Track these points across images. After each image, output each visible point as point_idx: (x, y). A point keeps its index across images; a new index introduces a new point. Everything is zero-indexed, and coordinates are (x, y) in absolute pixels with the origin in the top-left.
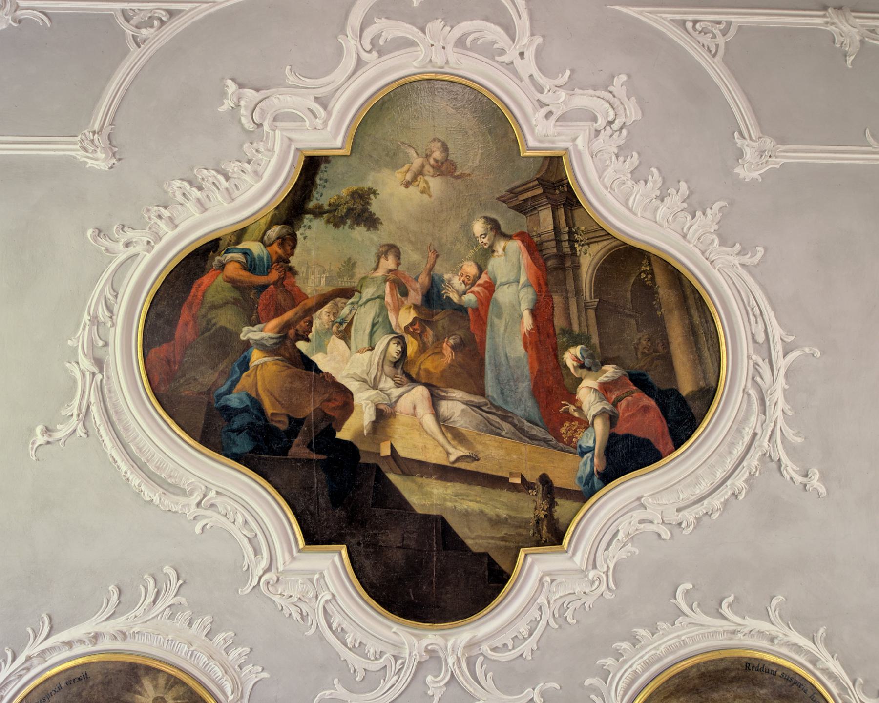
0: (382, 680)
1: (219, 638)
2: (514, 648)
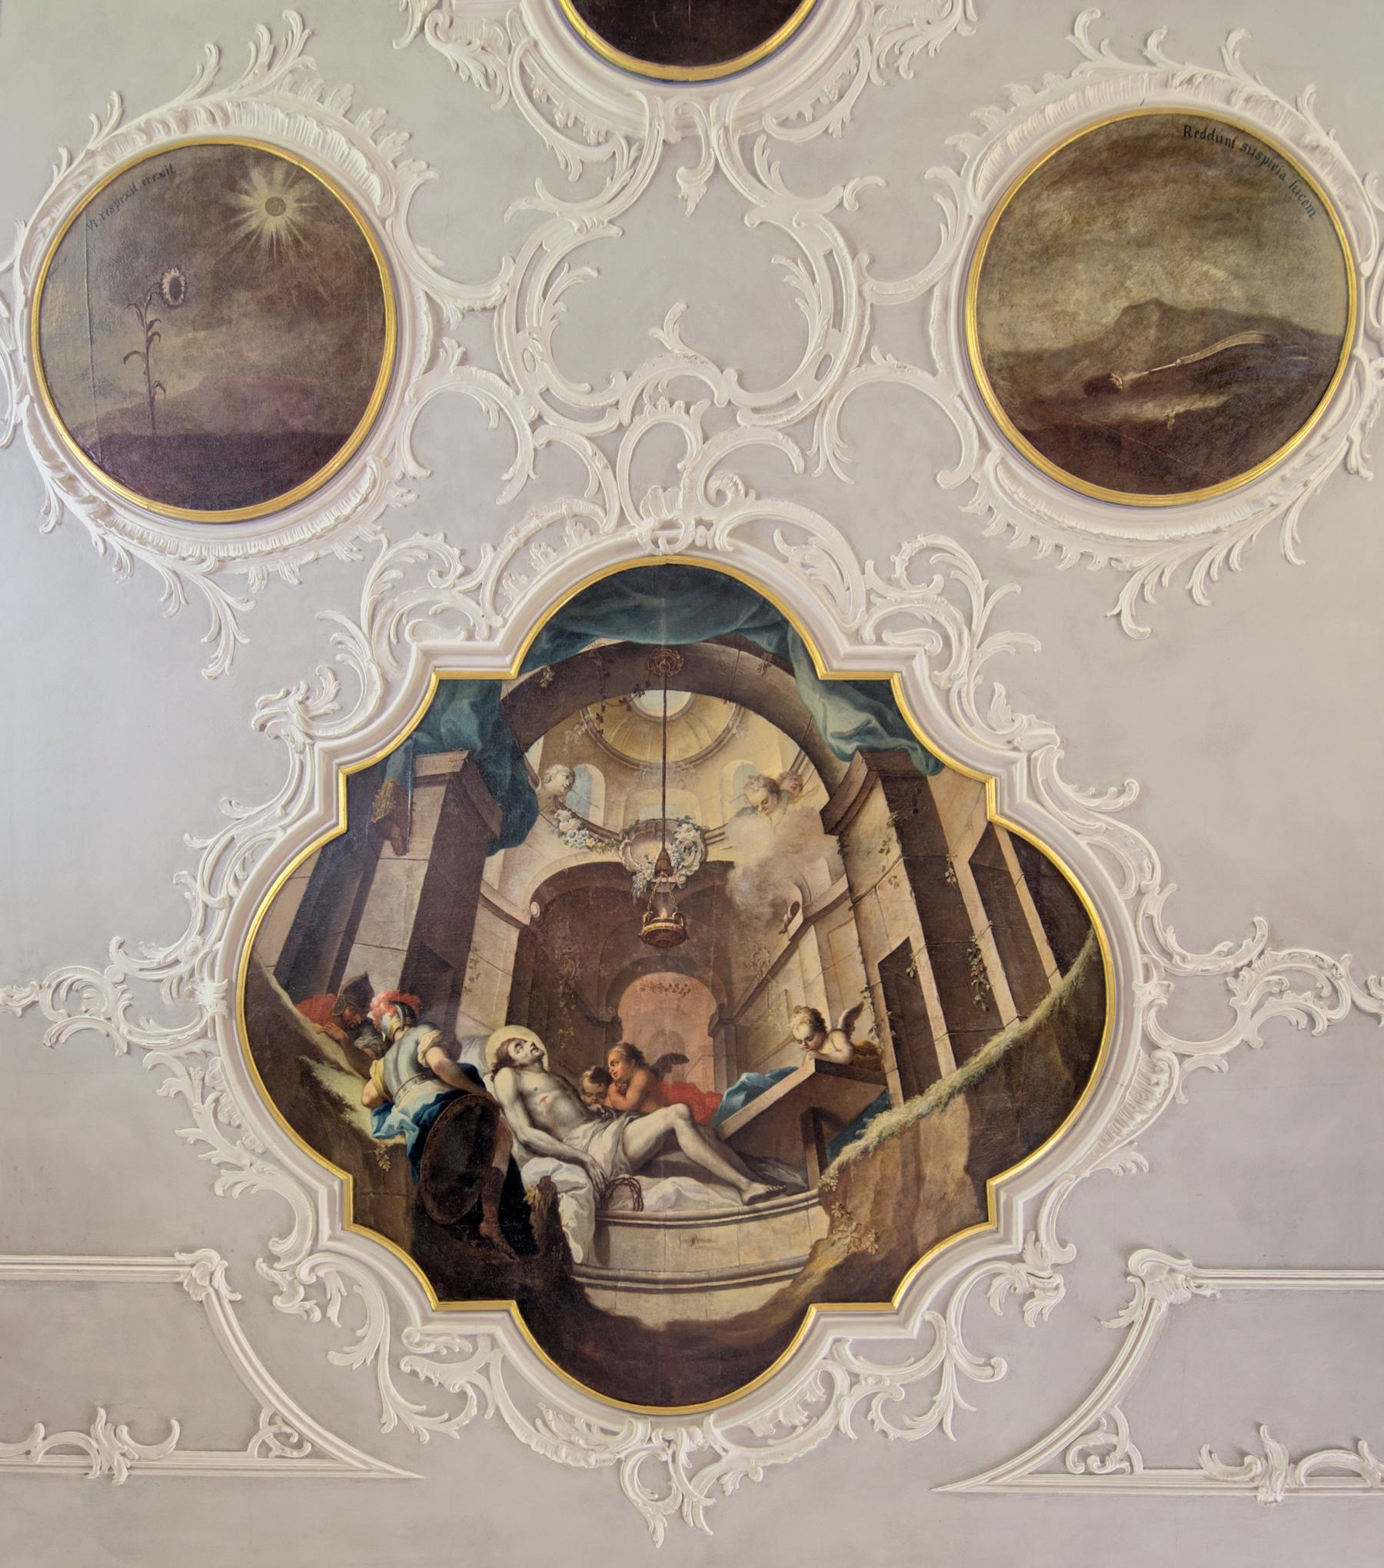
0: (608, 178)
1: (364, 118)
2: (814, 120)
